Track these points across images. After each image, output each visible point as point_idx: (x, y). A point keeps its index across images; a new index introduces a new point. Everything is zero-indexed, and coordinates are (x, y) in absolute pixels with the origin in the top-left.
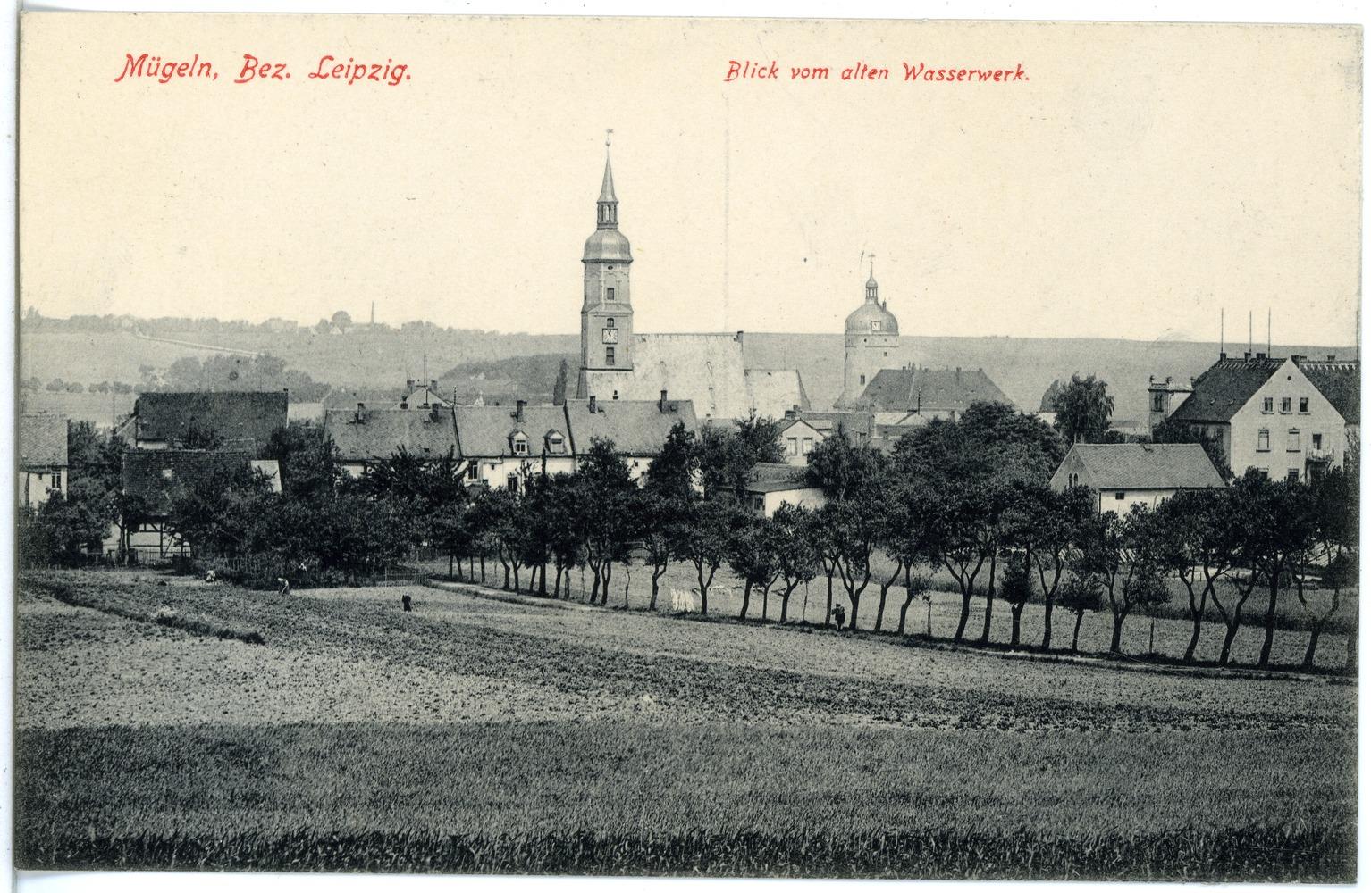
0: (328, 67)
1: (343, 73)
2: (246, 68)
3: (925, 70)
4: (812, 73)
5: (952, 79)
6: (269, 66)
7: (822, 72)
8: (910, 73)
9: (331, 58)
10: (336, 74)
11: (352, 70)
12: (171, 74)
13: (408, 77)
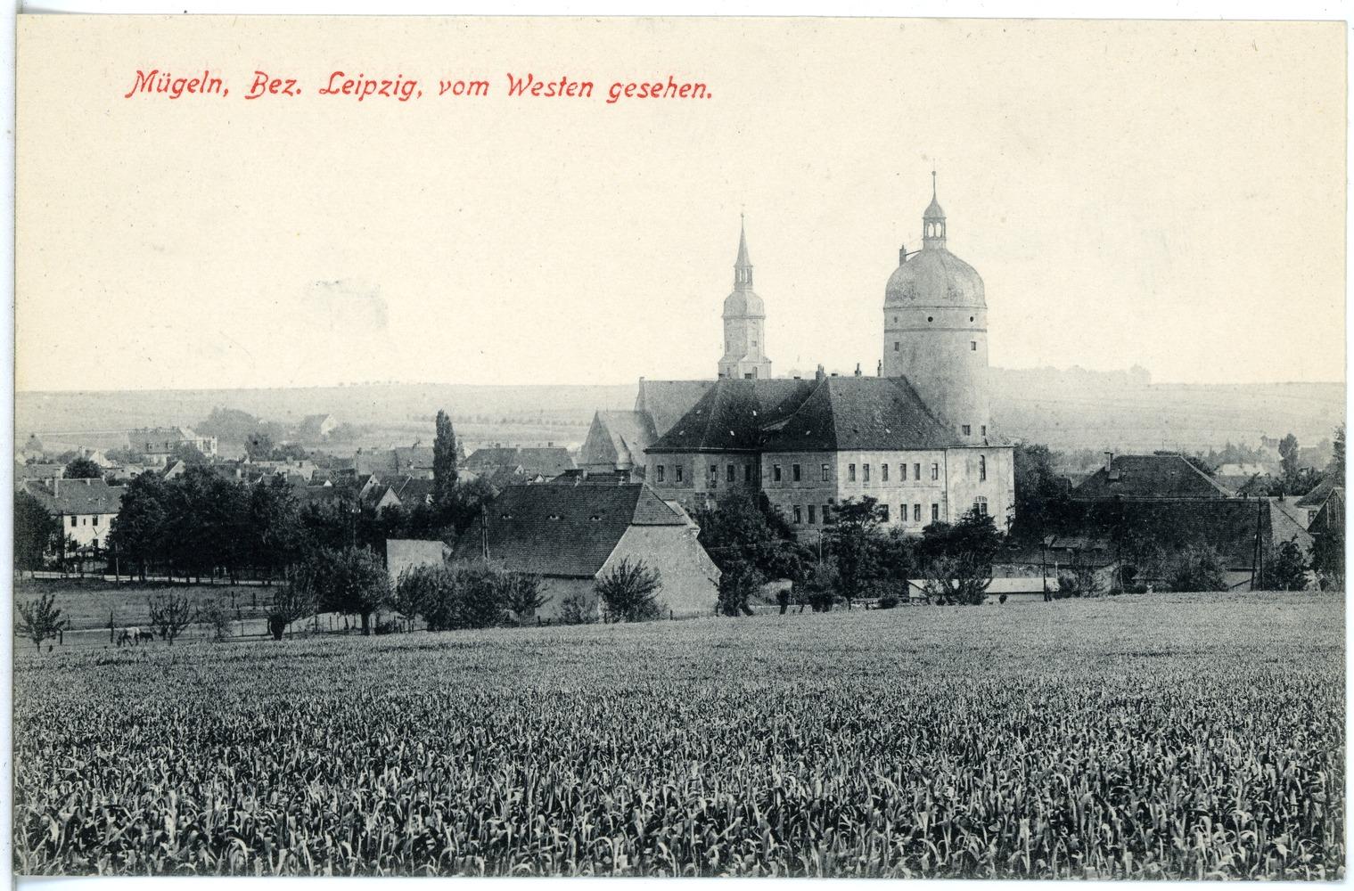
0: (339, 83)
1: (199, 86)
2: (256, 84)
3: (534, 82)
4: (467, 86)
5: (553, 94)
6: (280, 82)
7: (481, 86)
8: (515, 87)
9: (342, 74)
10: (347, 90)
11: (363, 85)
12: (181, 90)
13: (420, 94)
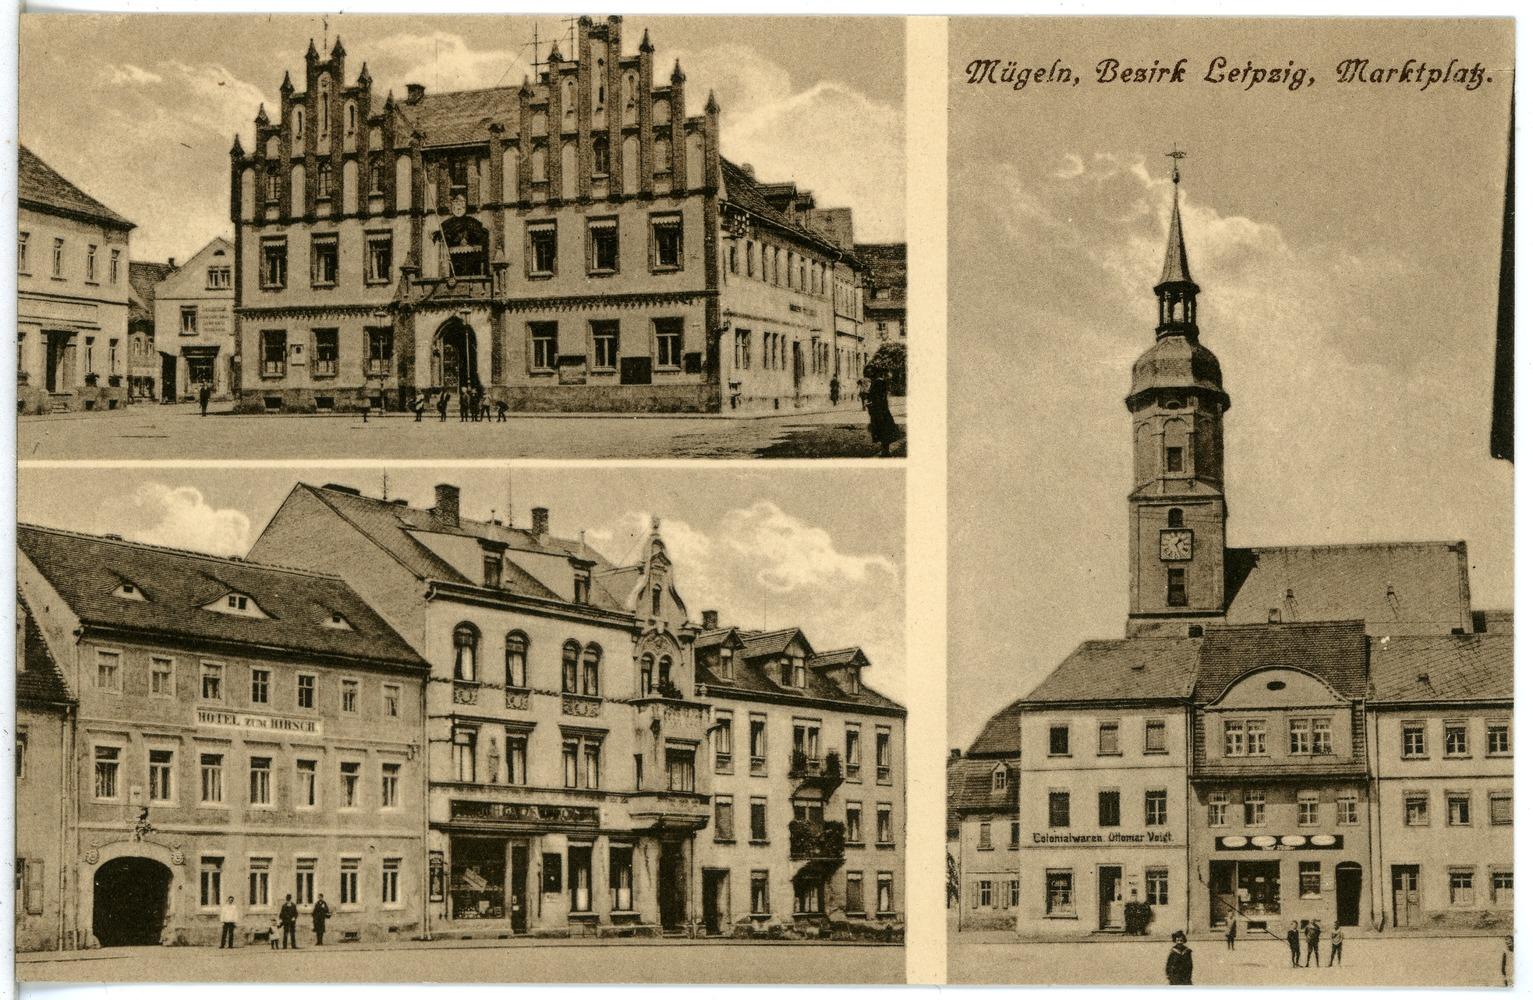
11: (1251, 74)
